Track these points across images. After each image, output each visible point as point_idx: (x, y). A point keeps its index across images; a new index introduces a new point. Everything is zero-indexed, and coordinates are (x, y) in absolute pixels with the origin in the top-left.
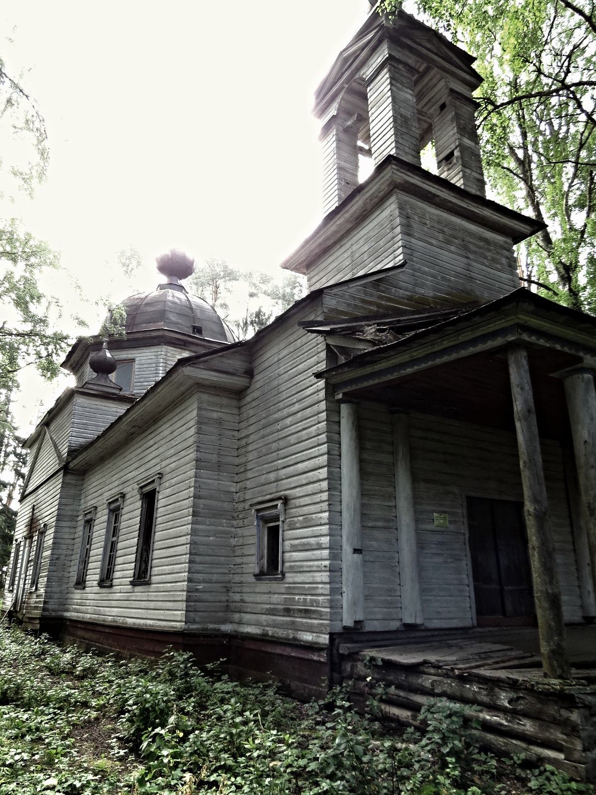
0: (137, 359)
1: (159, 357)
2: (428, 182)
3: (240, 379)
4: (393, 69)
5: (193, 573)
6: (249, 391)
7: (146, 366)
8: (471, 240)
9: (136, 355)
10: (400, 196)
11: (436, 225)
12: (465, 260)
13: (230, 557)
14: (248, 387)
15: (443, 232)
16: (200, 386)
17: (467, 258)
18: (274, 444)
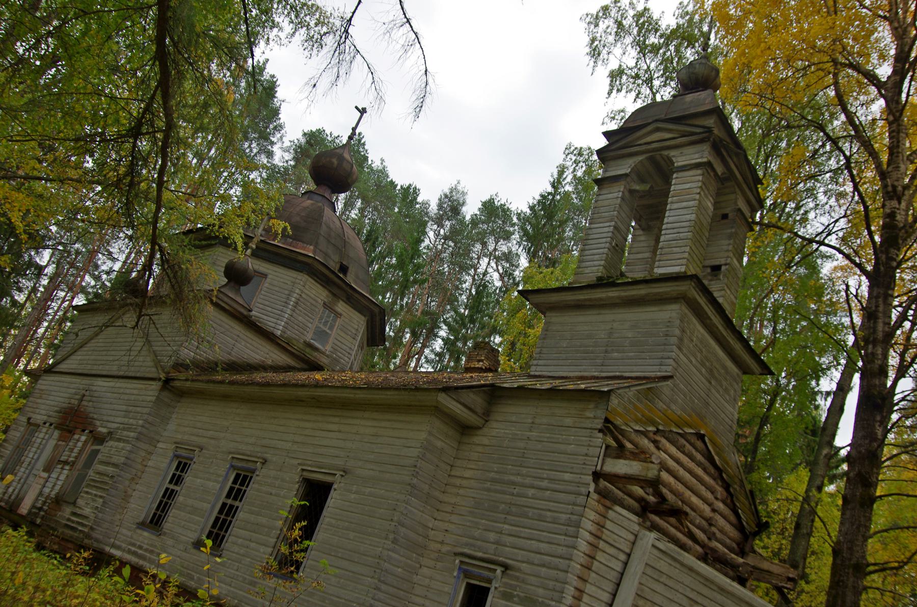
0: (270, 276)
1: (296, 285)
2: (710, 306)
3: (478, 419)
4: (706, 174)
5: (376, 600)
6: (480, 432)
7: (277, 289)
8: (717, 366)
9: (270, 272)
10: (683, 308)
11: (699, 344)
12: (707, 384)
13: (408, 592)
14: (480, 428)
15: (701, 352)
16: (439, 411)
17: (710, 383)
18: (503, 505)
